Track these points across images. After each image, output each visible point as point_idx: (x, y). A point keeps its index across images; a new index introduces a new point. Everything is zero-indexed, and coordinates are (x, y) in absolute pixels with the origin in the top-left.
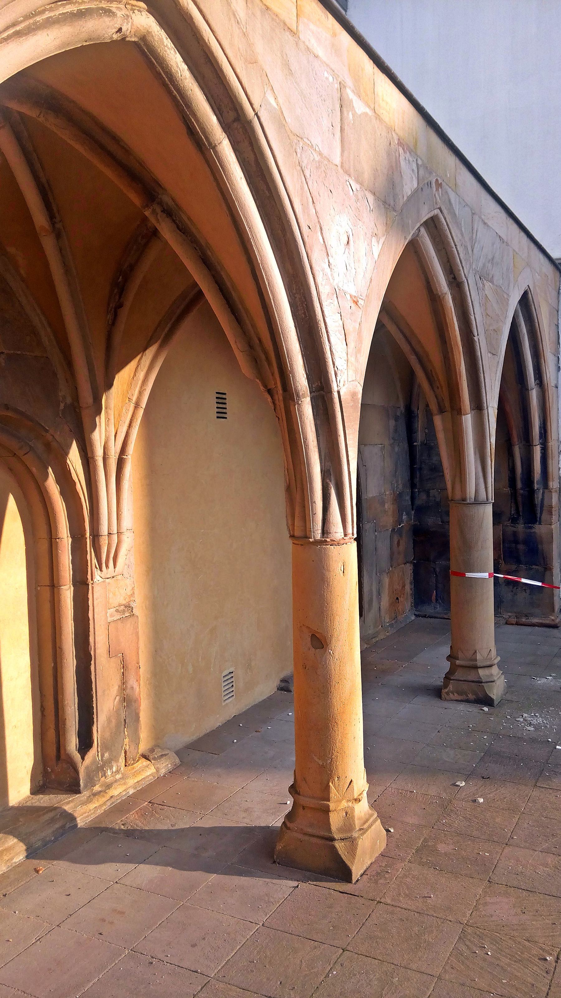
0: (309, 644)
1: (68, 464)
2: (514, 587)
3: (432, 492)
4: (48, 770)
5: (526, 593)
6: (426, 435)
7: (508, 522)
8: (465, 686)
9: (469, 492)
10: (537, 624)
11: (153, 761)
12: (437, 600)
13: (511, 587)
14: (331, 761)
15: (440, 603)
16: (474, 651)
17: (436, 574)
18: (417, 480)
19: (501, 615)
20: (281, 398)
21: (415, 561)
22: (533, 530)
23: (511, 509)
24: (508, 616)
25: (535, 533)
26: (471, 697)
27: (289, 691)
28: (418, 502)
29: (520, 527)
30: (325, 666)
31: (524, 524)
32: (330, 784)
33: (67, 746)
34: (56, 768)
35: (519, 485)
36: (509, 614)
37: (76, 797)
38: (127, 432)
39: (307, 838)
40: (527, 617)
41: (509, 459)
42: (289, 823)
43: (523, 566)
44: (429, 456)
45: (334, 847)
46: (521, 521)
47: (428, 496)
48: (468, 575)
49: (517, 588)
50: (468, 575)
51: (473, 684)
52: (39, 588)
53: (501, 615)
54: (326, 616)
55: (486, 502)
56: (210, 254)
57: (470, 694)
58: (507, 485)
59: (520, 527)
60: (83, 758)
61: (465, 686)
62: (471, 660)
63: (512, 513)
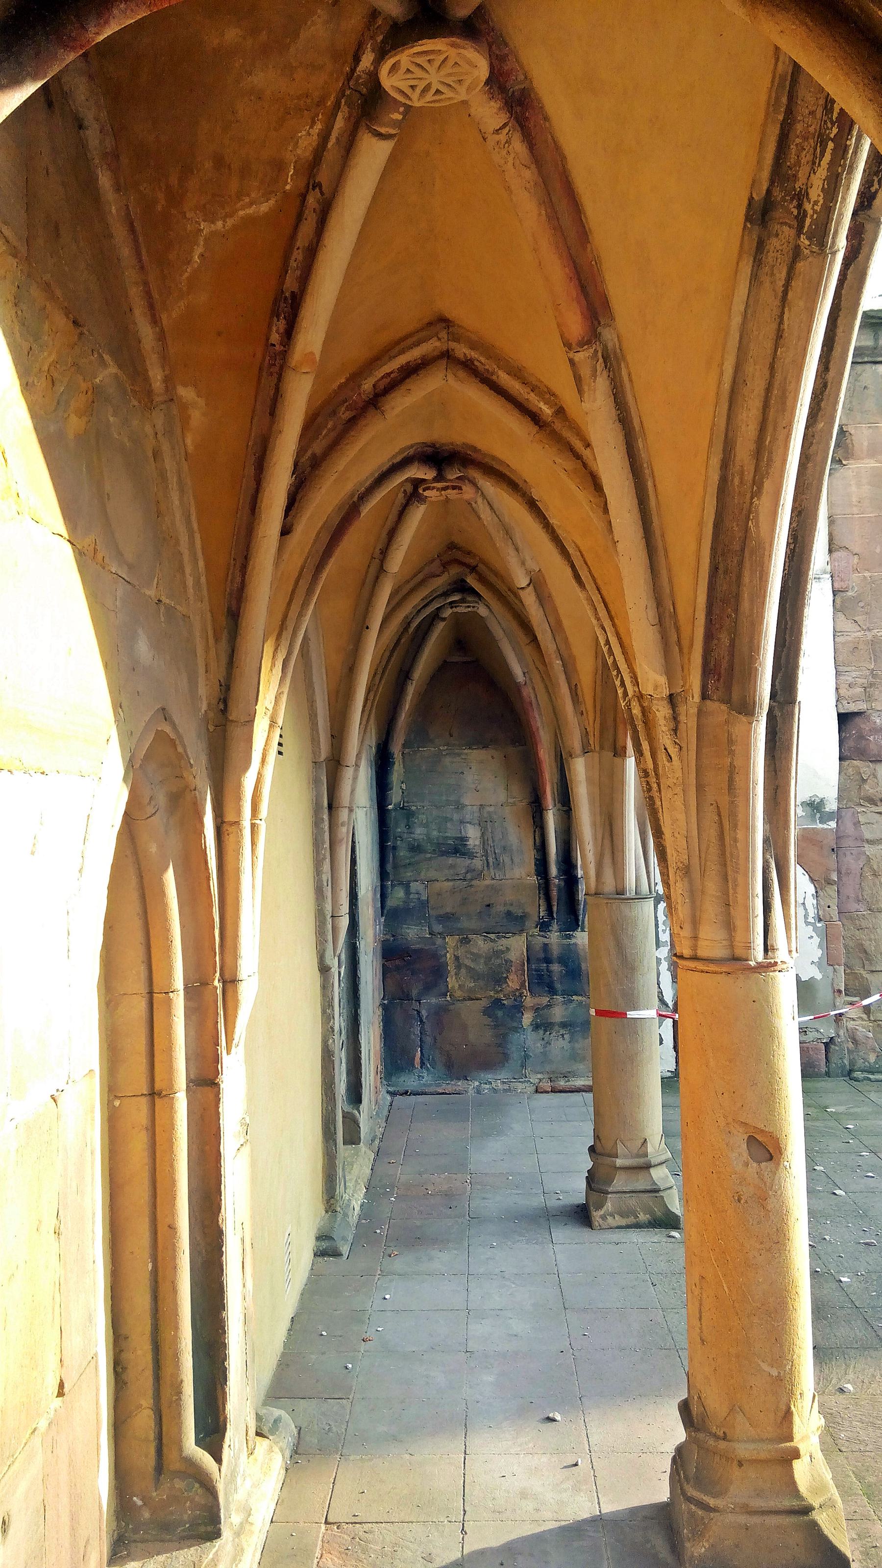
0: (746, 1154)
1: (204, 835)
2: (545, 1031)
3: (414, 886)
4: (135, 1502)
5: (564, 1039)
6: (403, 793)
7: (535, 930)
8: (632, 1202)
9: (629, 880)
10: (583, 1087)
11: (271, 1437)
12: (422, 1064)
13: (541, 1032)
14: (792, 1366)
15: (428, 1069)
16: (642, 1141)
17: (421, 1021)
18: (389, 867)
19: (526, 1080)
20: (694, 711)
21: (386, 1002)
22: (573, 941)
23: (539, 909)
24: (537, 1080)
25: (575, 944)
26: (643, 1217)
27: (337, 1254)
28: (391, 903)
29: (554, 937)
30: (779, 1192)
31: (560, 932)
32: (792, 1407)
33: (184, 1440)
34: (154, 1494)
35: (554, 870)
36: (539, 1076)
37: (217, 1547)
38: (259, 773)
39: (756, 1520)
40: (566, 1079)
41: (535, 831)
42: (712, 1500)
43: (559, 998)
44: (409, 826)
45: (814, 1524)
46: (555, 926)
47: (408, 892)
48: (631, 1014)
49: (550, 1034)
50: (631, 1014)
51: (647, 1195)
52: (117, 1103)
53: (526, 1080)
54: (778, 1101)
55: (649, 896)
56: (641, 445)
57: (641, 1214)
58: (533, 871)
59: (554, 937)
60: (218, 1460)
61: (632, 1202)
62: (638, 1156)
63: (541, 914)
